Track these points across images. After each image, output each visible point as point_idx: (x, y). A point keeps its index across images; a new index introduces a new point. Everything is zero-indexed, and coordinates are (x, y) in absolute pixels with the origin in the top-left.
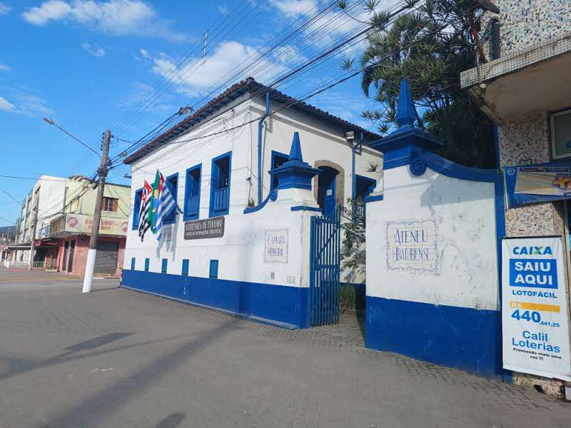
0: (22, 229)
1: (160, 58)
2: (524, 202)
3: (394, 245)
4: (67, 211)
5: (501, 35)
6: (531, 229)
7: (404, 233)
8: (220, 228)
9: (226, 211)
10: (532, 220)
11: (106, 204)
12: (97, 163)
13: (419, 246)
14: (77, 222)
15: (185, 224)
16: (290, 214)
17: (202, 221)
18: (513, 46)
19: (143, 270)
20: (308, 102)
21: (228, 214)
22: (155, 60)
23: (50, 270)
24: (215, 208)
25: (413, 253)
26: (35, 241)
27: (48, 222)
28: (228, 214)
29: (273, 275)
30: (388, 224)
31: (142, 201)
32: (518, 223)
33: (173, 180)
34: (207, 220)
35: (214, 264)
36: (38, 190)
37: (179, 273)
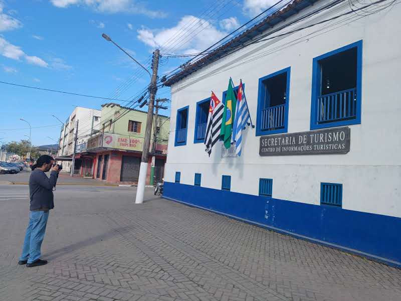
0: (61, 146)
1: (141, 29)
4: (106, 130)
8: (340, 142)
9: (353, 114)
11: (132, 127)
12: (146, 82)
14: (111, 140)
17: (296, 135)
19: (193, 184)
21: (359, 122)
22: (138, 30)
26: (76, 154)
27: (86, 140)
28: (359, 122)
31: (210, 113)
34: (308, 134)
35: (198, 177)
36: (74, 118)
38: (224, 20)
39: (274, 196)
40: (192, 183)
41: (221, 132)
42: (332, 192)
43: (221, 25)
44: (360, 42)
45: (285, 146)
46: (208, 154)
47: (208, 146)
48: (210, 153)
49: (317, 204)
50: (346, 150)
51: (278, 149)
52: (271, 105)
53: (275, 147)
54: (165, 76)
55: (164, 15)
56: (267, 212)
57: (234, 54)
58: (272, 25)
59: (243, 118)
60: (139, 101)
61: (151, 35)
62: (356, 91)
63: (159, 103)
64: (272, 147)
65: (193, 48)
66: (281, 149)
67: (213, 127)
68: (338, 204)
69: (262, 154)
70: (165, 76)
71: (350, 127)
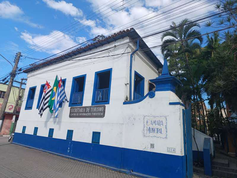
1: (24, 32)
2: (193, 113)
8: (101, 112)
17: (86, 107)
24: (72, 103)
29: (152, 146)
31: (44, 93)
33: (64, 81)
34: (90, 107)
35: (36, 129)
37: (21, 132)
38: (79, 37)
39: (73, 140)
41: (49, 104)
42: (96, 135)
43: (77, 40)
44: (111, 69)
45: (81, 113)
46: (40, 116)
47: (40, 111)
48: (41, 115)
49: (161, 148)
50: (103, 116)
51: (78, 114)
52: (100, 89)
53: (76, 113)
54: (21, 68)
55: (41, 27)
56: (69, 148)
57: (58, 64)
58: (80, 53)
59: (60, 97)
60: (3, 80)
61: (31, 37)
62: (82, 93)
63: (23, 81)
64: (75, 113)
65: (58, 49)
66: (79, 114)
67: (45, 101)
68: (97, 142)
69: (71, 116)
70: (21, 68)
71: (106, 105)
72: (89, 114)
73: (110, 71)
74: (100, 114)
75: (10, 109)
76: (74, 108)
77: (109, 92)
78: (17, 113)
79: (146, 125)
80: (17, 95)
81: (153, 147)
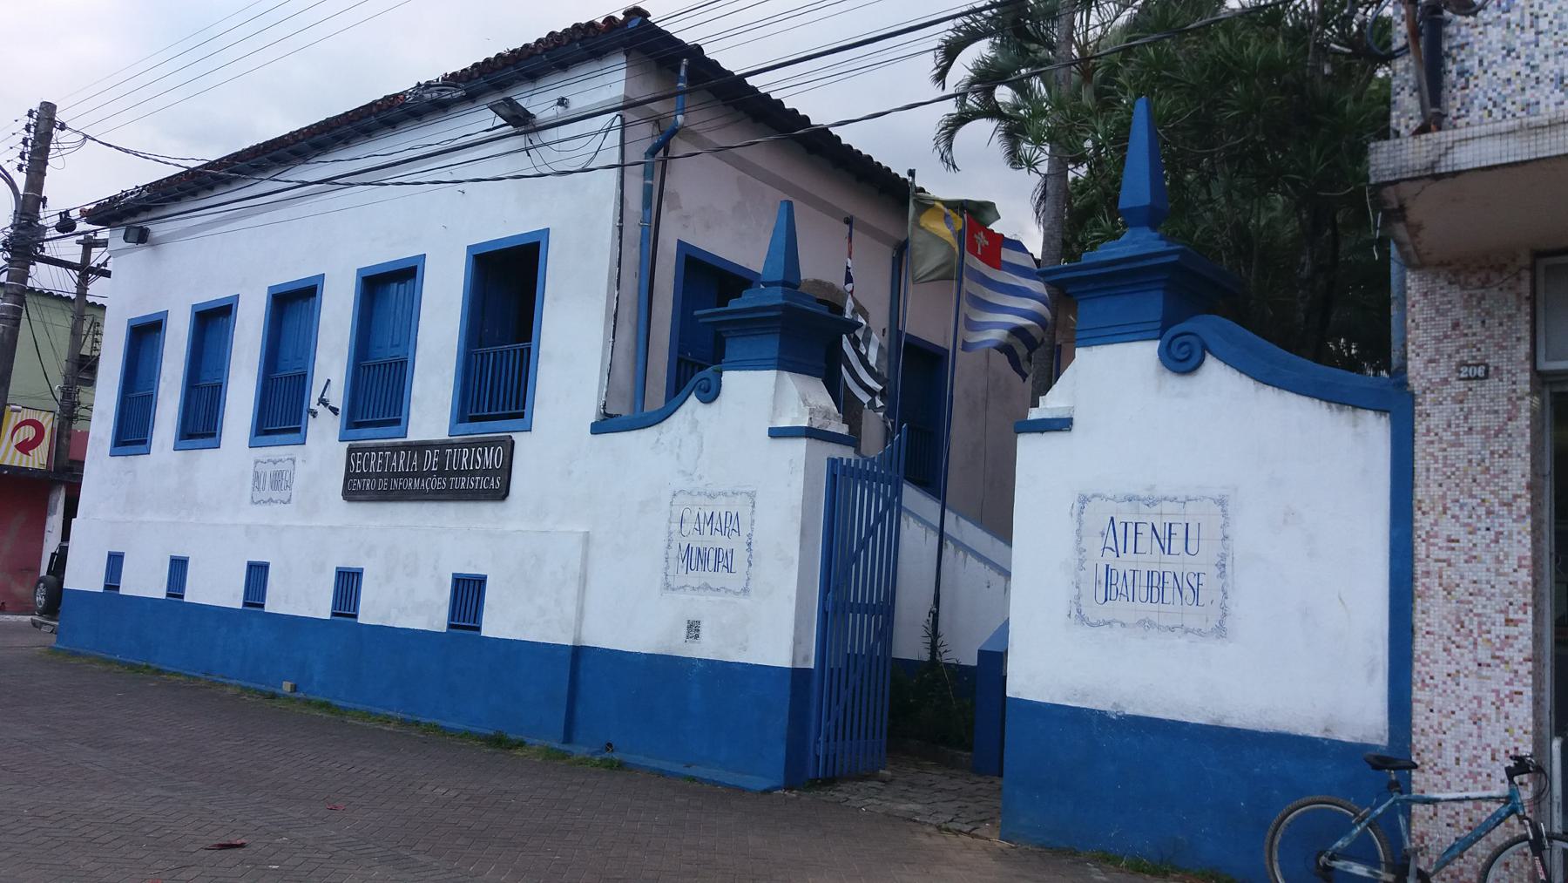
3: (1099, 559)
5: (1445, 47)
6: (1476, 538)
7: (1131, 529)
10: (1479, 517)
13: (1172, 564)
15: (350, 450)
16: (756, 439)
17: (421, 447)
18: (1472, 83)
19: (160, 593)
20: (847, 136)
23: (350, 705)
25: (1156, 585)
29: (693, 629)
30: (1084, 500)
32: (1446, 521)
33: (407, 274)
34: (442, 445)
35: (257, 573)
37: (97, 586)
40: (320, 606)
42: (468, 593)
45: (460, 473)
72: (438, 483)
73: (538, 244)
74: (488, 482)
75: (24, 447)
76: (364, 449)
77: (636, 362)
78: (66, 474)
79: (676, 536)
80: (64, 353)
81: (697, 637)
